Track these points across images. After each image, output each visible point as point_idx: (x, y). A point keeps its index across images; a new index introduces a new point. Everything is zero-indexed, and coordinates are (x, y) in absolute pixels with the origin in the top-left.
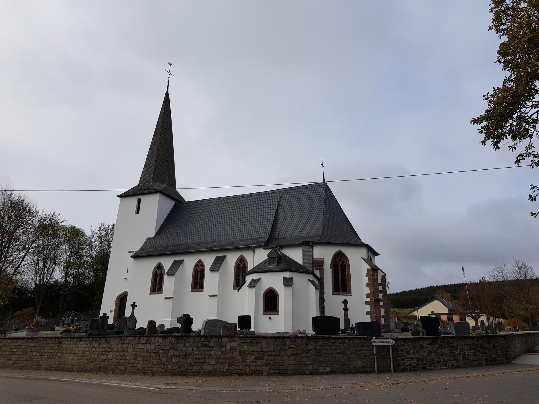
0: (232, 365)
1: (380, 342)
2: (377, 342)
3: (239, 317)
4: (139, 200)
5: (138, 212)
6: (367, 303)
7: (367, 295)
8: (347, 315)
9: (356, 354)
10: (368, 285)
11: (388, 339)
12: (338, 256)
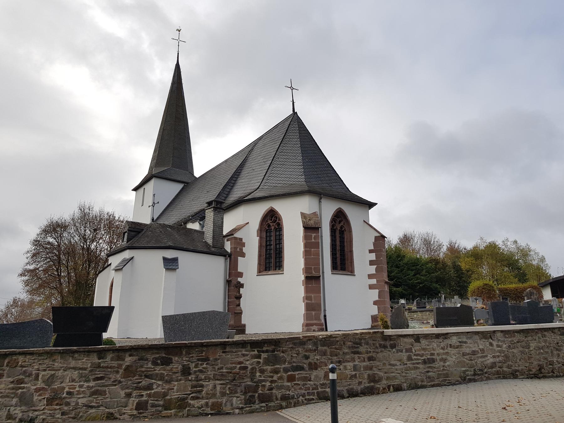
3: (165, 318)
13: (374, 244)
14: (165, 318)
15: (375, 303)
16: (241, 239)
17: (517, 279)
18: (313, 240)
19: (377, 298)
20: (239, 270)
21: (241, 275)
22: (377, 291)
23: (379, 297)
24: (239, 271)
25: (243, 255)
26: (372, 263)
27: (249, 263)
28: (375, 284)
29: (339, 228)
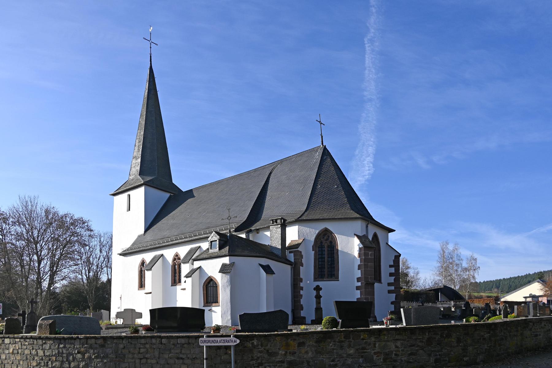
0: (411, 354)
1: (213, 341)
2: (209, 341)
3: (150, 310)
4: (129, 196)
5: (129, 209)
6: (358, 288)
7: (359, 280)
8: (320, 303)
9: (178, 358)
10: (359, 267)
11: (230, 336)
12: (325, 235)
14: (150, 310)
21: (301, 280)
22: (394, 295)
23: (396, 299)
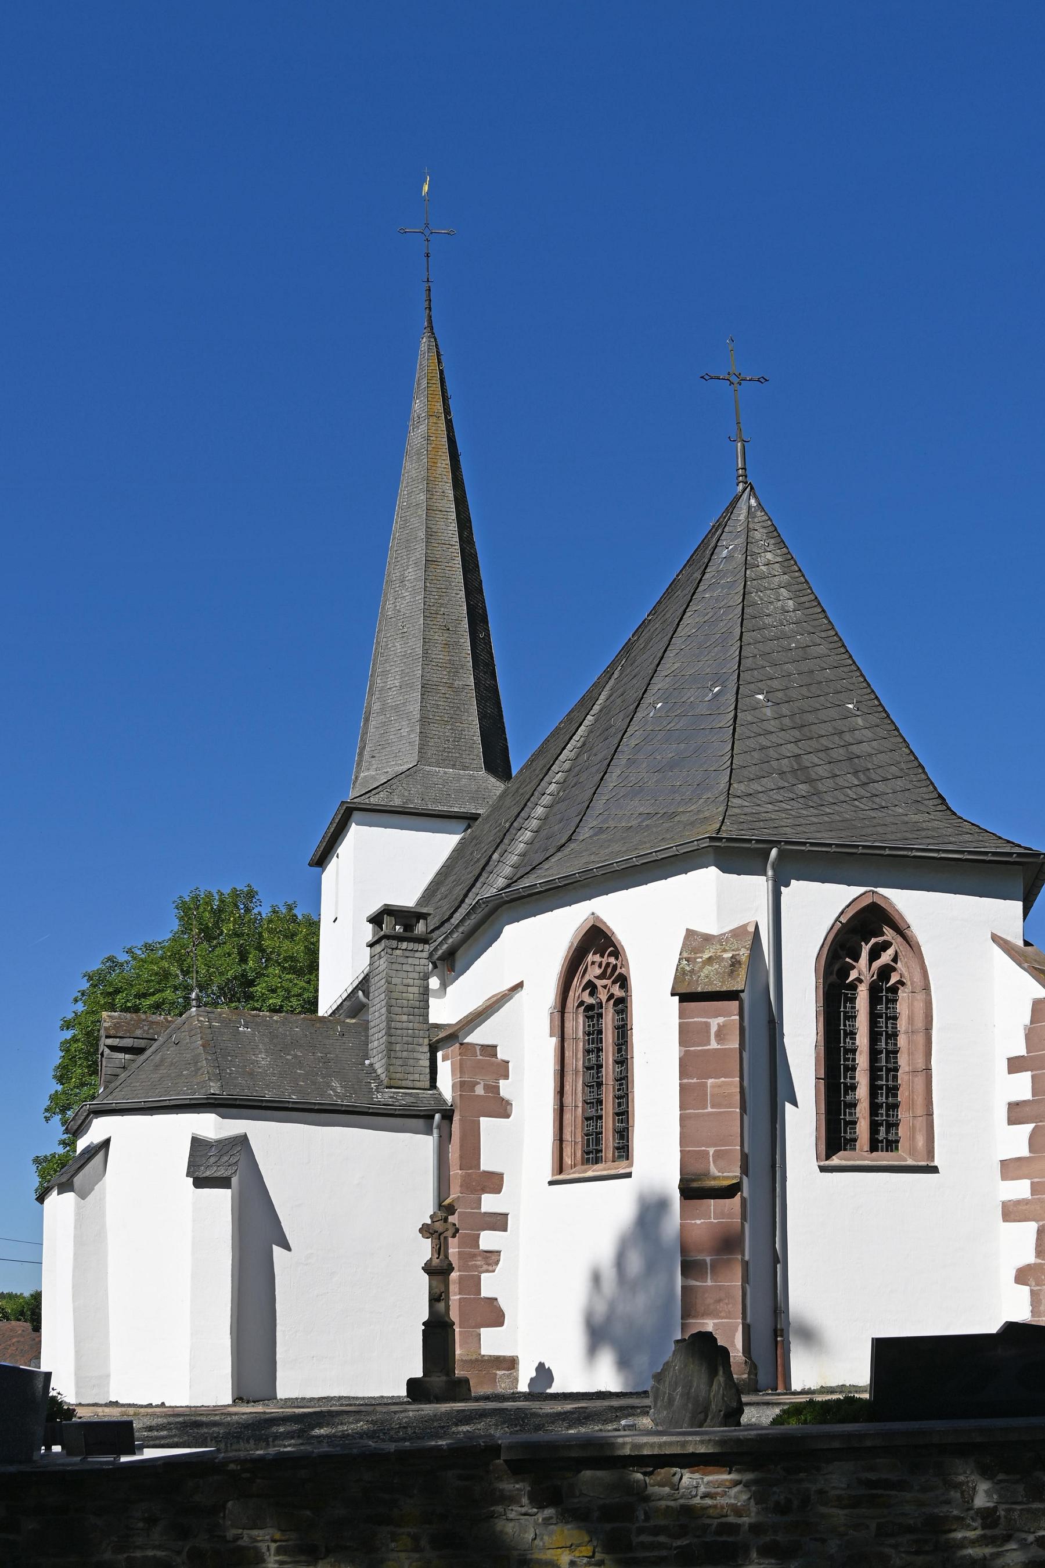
13: (1031, 1036)
15: (1022, 1276)
16: (490, 1050)
17: (252, 1442)
18: (714, 1045)
19: (1029, 1257)
20: (486, 1164)
22: (1029, 1230)
24: (484, 1167)
25: (502, 1109)
26: (1016, 1113)
27: (521, 1140)
28: (1025, 1202)
29: (867, 978)
